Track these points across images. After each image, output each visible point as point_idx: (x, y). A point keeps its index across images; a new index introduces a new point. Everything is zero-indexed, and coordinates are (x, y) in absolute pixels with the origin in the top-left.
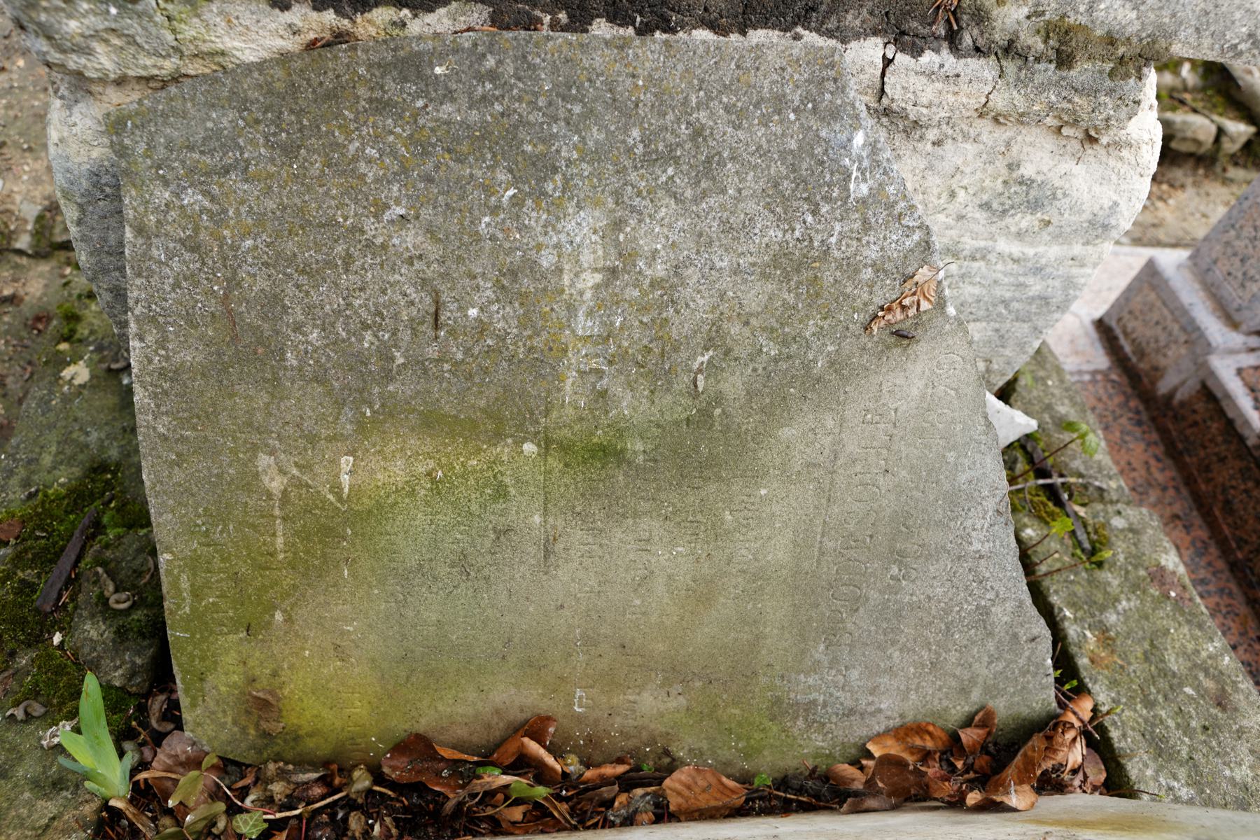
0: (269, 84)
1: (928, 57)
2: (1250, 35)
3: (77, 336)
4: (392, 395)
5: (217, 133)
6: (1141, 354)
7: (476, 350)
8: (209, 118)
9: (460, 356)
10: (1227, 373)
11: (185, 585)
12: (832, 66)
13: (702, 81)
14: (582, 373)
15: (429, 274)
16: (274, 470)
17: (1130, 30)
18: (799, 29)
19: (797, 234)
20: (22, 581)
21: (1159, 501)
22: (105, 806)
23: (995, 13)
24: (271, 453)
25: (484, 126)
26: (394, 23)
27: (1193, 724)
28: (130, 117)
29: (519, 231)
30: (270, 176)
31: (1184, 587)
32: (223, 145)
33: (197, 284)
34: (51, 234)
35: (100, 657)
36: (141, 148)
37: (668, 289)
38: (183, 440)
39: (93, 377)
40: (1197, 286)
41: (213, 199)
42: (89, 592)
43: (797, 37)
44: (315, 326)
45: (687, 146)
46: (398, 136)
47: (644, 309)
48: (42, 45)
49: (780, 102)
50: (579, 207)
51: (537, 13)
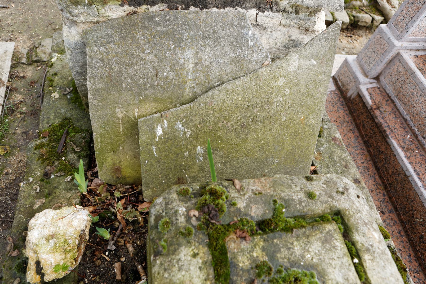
0: (119, 23)
1: (266, 13)
2: (340, 6)
3: (54, 85)
4: (147, 94)
5: (108, 34)
6: (343, 85)
7: (166, 83)
8: (106, 31)
9: (162, 84)
10: (364, 90)
11: (99, 141)
12: (243, 16)
13: (215, 20)
14: (190, 88)
15: (155, 65)
16: (120, 112)
17: (312, 5)
18: (237, 7)
19: (238, 54)
20: (52, 146)
21: (347, 126)
22: (82, 194)
23: (280, 3)
24: (119, 108)
25: (167, 31)
26: (146, 9)
27: (339, 172)
28: (88, 31)
29: (175, 55)
30: (119, 44)
31: (340, 141)
32: (109, 37)
33: (103, 69)
34: (32, 58)
35: (75, 162)
36: (91, 38)
37: (209, 68)
38: (99, 105)
39: (60, 96)
40: (358, 66)
41: (106, 49)
42: (69, 148)
43: (236, 9)
44: (129, 78)
45: (212, 35)
46: (148, 34)
47: (204, 72)
48: (68, 15)
49: (232, 25)
50: (188, 49)
51: (178, 5)
